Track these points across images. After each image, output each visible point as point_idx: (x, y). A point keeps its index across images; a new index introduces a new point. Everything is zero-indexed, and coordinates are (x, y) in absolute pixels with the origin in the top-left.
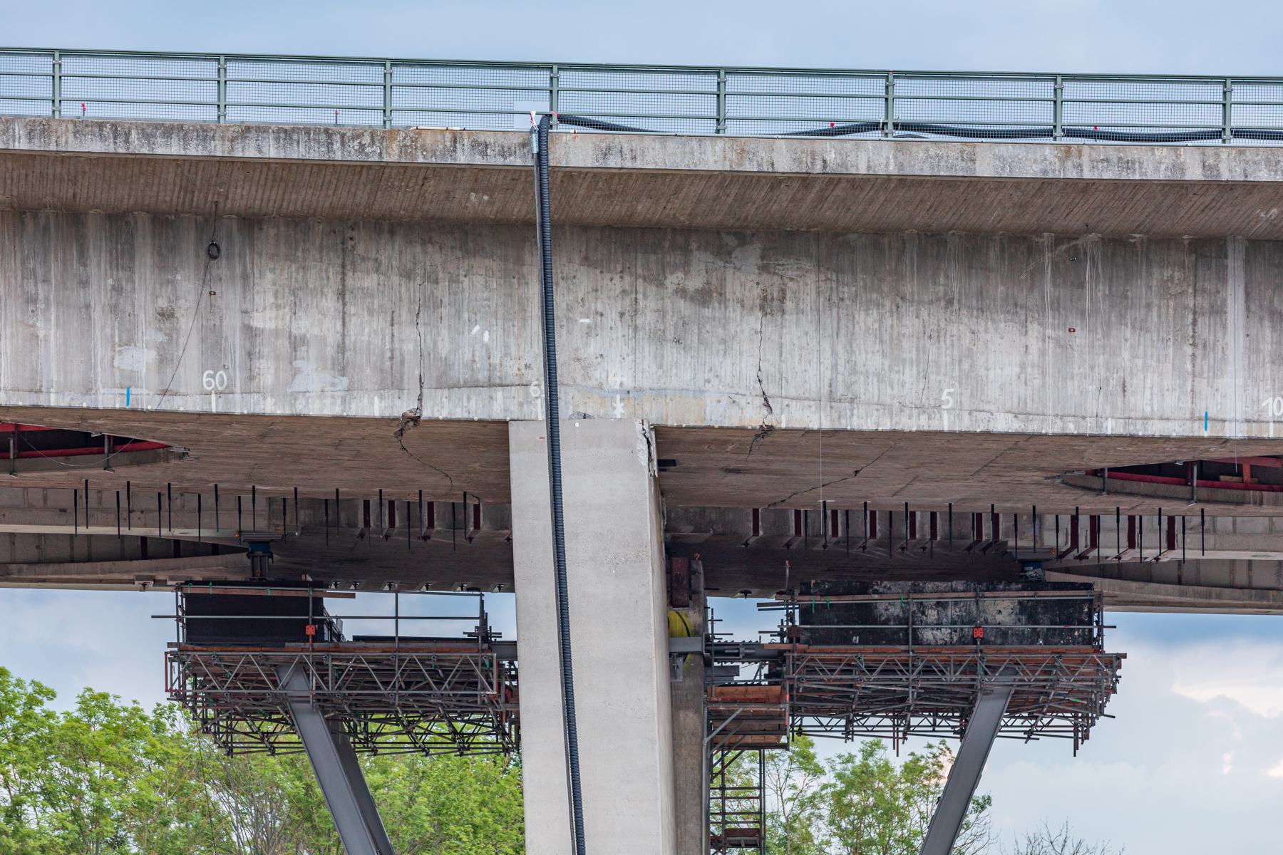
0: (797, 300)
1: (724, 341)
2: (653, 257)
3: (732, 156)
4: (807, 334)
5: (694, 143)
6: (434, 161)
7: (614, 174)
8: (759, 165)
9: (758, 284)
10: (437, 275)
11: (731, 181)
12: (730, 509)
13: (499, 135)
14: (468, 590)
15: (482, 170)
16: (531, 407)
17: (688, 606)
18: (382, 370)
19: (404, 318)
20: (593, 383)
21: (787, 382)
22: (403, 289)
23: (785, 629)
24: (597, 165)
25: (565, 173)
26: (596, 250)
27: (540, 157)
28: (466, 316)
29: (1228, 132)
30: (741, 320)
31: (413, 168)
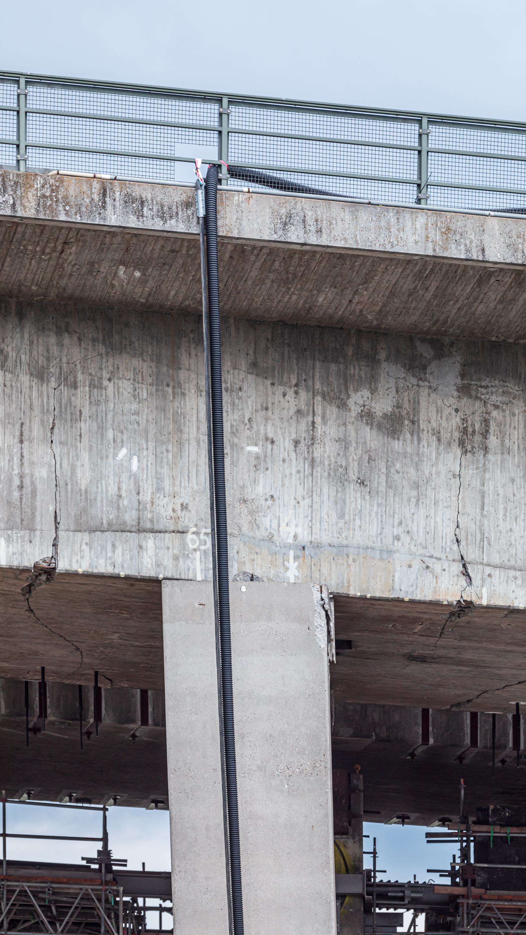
0: (502, 435)
1: (416, 486)
2: (333, 367)
3: (436, 236)
4: (513, 481)
5: (391, 214)
6: (78, 219)
7: (295, 252)
8: (468, 251)
9: (457, 411)
10: (75, 377)
11: (432, 270)
12: (370, 704)
13: (158, 188)
14: (77, 801)
15: (136, 235)
16: (189, 562)
17: (346, 833)
18: (9, 503)
19: (35, 433)
20: (261, 534)
21: (489, 544)
22: (35, 394)
23: (457, 868)
24: (275, 237)
25: (236, 246)
26: (266, 353)
28: (110, 434)
30: (437, 458)
31: (53, 228)
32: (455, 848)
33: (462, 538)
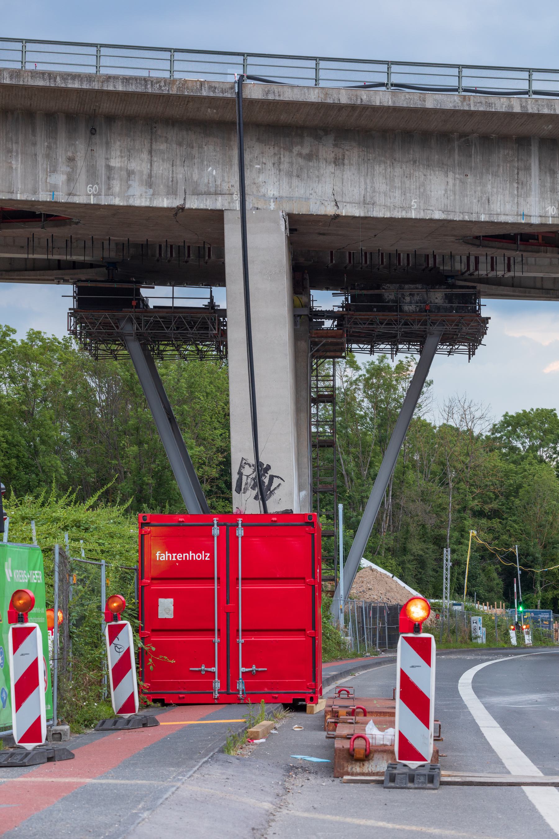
1: (318, 177)
2: (287, 139)
4: (354, 174)
5: (306, 90)
7: (271, 102)
8: (334, 100)
14: (205, 285)
19: (178, 163)
20: (261, 194)
22: (178, 151)
24: (263, 98)
27: (239, 94)
28: (205, 163)
29: (531, 92)
32: (343, 298)
33: (335, 193)
